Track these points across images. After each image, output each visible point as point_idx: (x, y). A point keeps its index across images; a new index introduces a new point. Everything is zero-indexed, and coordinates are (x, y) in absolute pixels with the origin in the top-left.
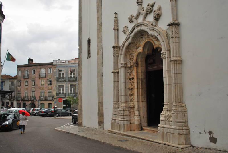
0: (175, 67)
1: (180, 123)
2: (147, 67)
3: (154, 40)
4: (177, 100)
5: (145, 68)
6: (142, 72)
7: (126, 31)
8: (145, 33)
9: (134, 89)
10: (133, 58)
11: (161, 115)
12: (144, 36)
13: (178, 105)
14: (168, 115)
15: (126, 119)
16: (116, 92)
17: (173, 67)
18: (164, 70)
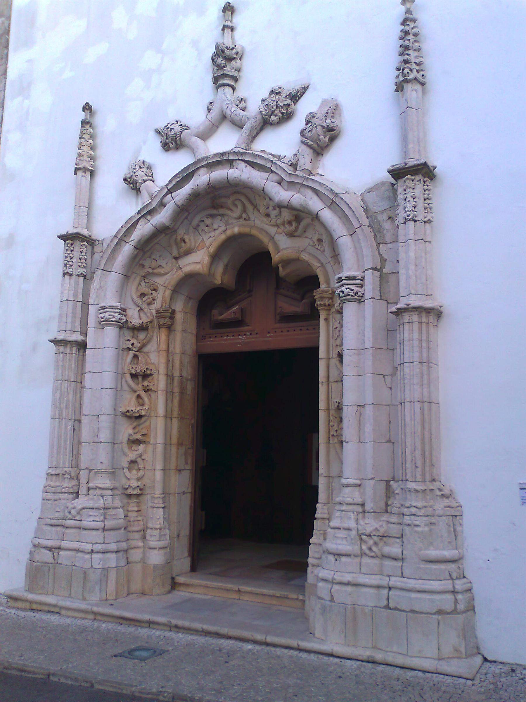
0: (424, 337)
1: (443, 566)
2: (200, 337)
3: (272, 230)
4: (427, 469)
5: (194, 339)
6: (183, 353)
7: (145, 181)
8: (232, 198)
9: (150, 417)
12: (221, 211)
13: (431, 490)
14: (376, 530)
15: (113, 547)
16: (66, 426)
17: (416, 336)
18: (322, 353)
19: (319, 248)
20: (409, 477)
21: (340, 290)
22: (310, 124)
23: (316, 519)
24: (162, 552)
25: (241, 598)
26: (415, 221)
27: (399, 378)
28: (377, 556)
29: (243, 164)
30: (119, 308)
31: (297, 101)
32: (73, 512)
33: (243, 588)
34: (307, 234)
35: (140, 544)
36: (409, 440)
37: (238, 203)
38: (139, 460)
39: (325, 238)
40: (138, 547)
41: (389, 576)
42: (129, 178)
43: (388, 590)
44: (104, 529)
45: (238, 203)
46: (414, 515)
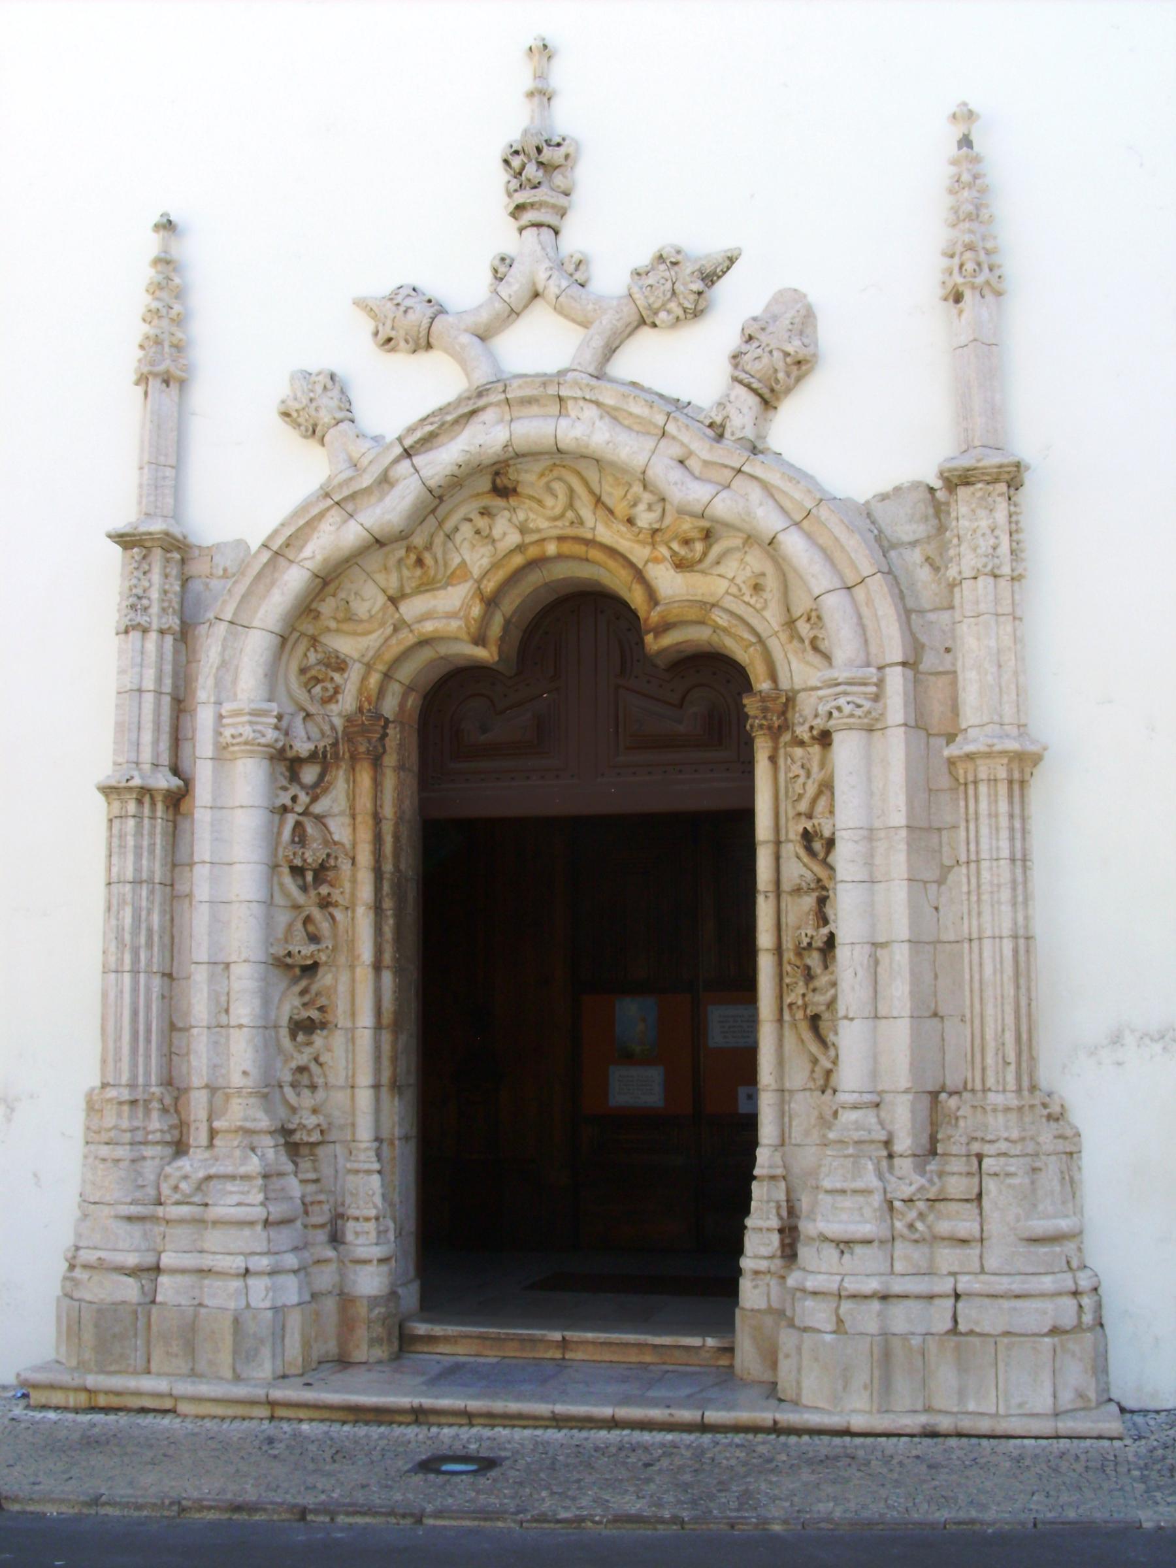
0: (1017, 811)
10: (337, 676)
11: (755, 1185)
13: (1032, 1107)
17: (1003, 807)
19: (752, 601)
20: (991, 1082)
21: (834, 703)
22: (756, 344)
23: (754, 1178)
24: (384, 1268)
25: (567, 1357)
26: (996, 576)
27: (965, 889)
28: (924, 1240)
29: (591, 412)
30: (247, 710)
31: (713, 283)
32: (184, 1186)
33: (573, 1335)
34: (721, 569)
35: (330, 1253)
36: (990, 1011)
37: (558, 487)
38: (314, 1067)
39: (771, 583)
40: (327, 1261)
41: (954, 1274)
42: (297, 411)
43: (952, 1301)
44: (267, 1223)
45: (558, 487)
46: (1005, 1154)
